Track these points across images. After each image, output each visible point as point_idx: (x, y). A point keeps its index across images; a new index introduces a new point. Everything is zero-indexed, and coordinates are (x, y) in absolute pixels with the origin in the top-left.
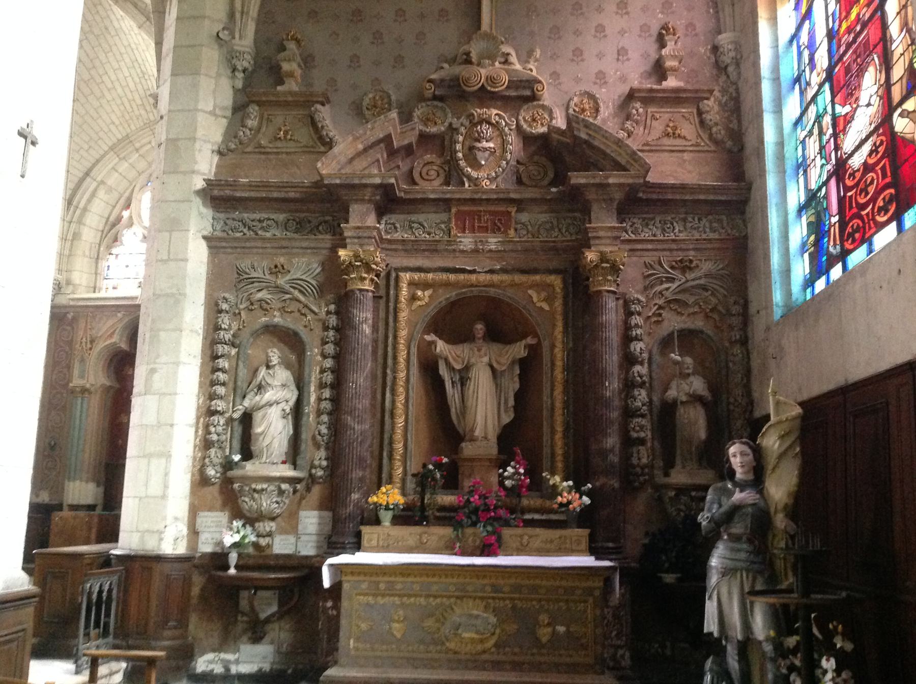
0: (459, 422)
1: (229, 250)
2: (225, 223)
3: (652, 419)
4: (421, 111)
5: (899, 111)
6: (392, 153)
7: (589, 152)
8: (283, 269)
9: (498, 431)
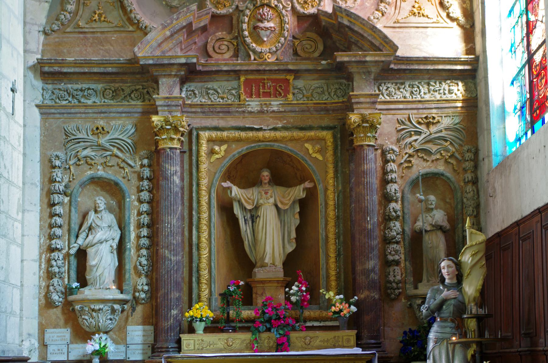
0: (251, 251)
1: (58, 116)
2: (53, 93)
3: (404, 245)
7: (350, 33)
8: (103, 130)
9: (283, 258)
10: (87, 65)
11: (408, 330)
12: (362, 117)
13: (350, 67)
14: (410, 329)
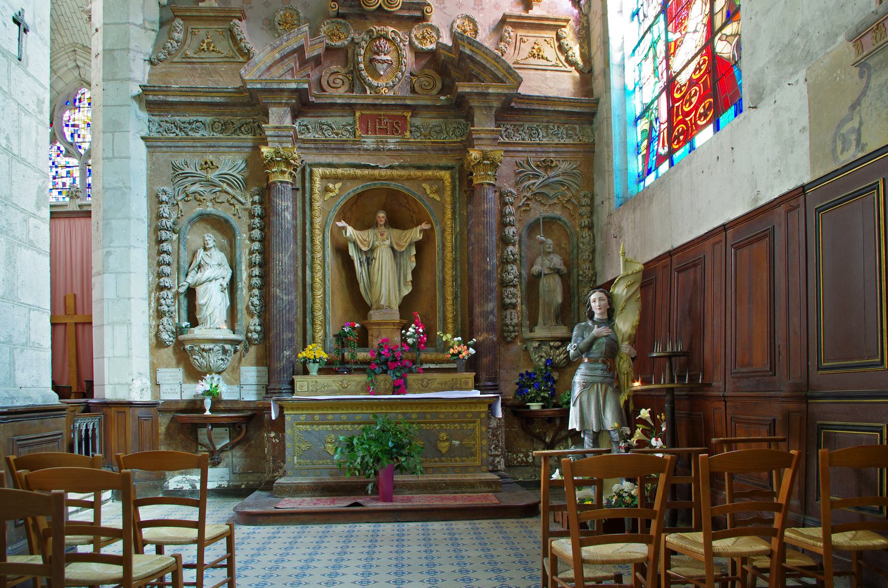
1: (165, 149)
2: (159, 125)
3: (521, 288)
4: (327, 26)
5: (719, 35)
6: (303, 62)
8: (212, 164)
10: (193, 94)
11: (524, 372)
12: (483, 154)
13: (471, 101)
14: (527, 372)
